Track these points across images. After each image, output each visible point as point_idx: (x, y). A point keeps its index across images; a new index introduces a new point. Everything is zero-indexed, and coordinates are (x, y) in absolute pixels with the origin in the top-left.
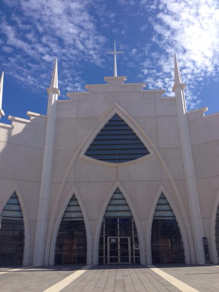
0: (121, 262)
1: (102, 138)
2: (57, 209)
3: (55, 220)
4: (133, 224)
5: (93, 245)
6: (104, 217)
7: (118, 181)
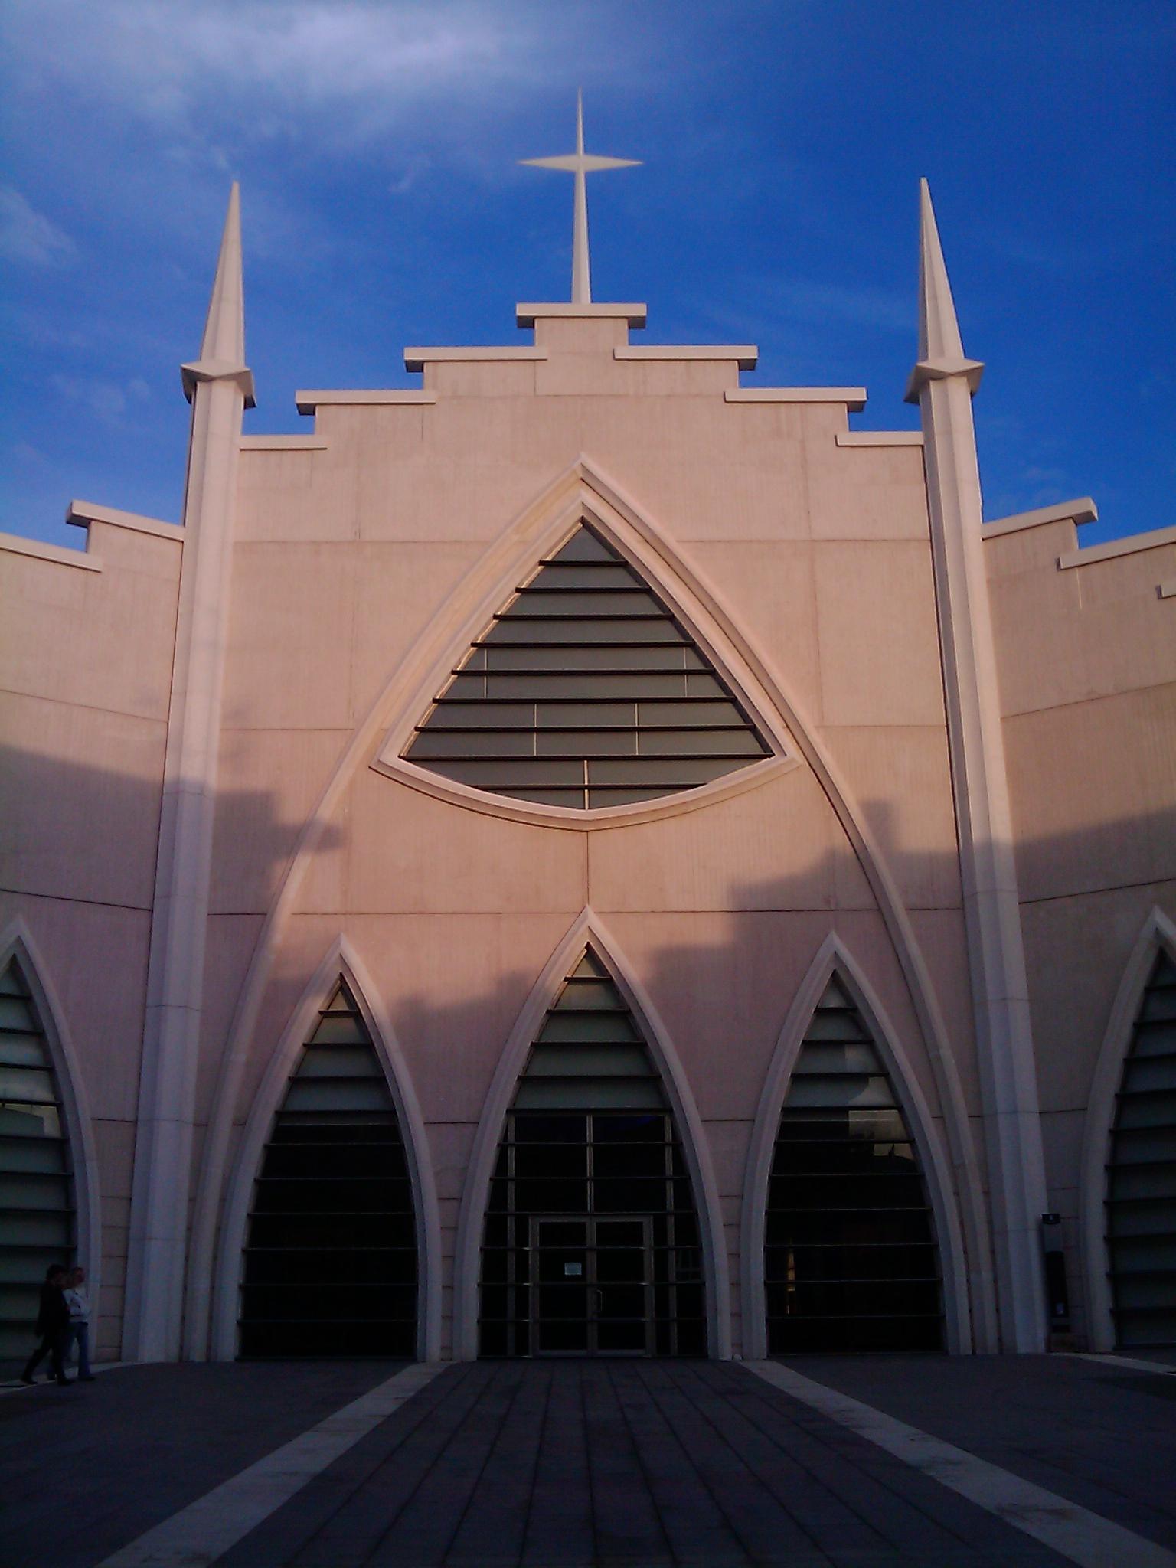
1: (483, 688)
3: (241, 1124)
4: (669, 1153)
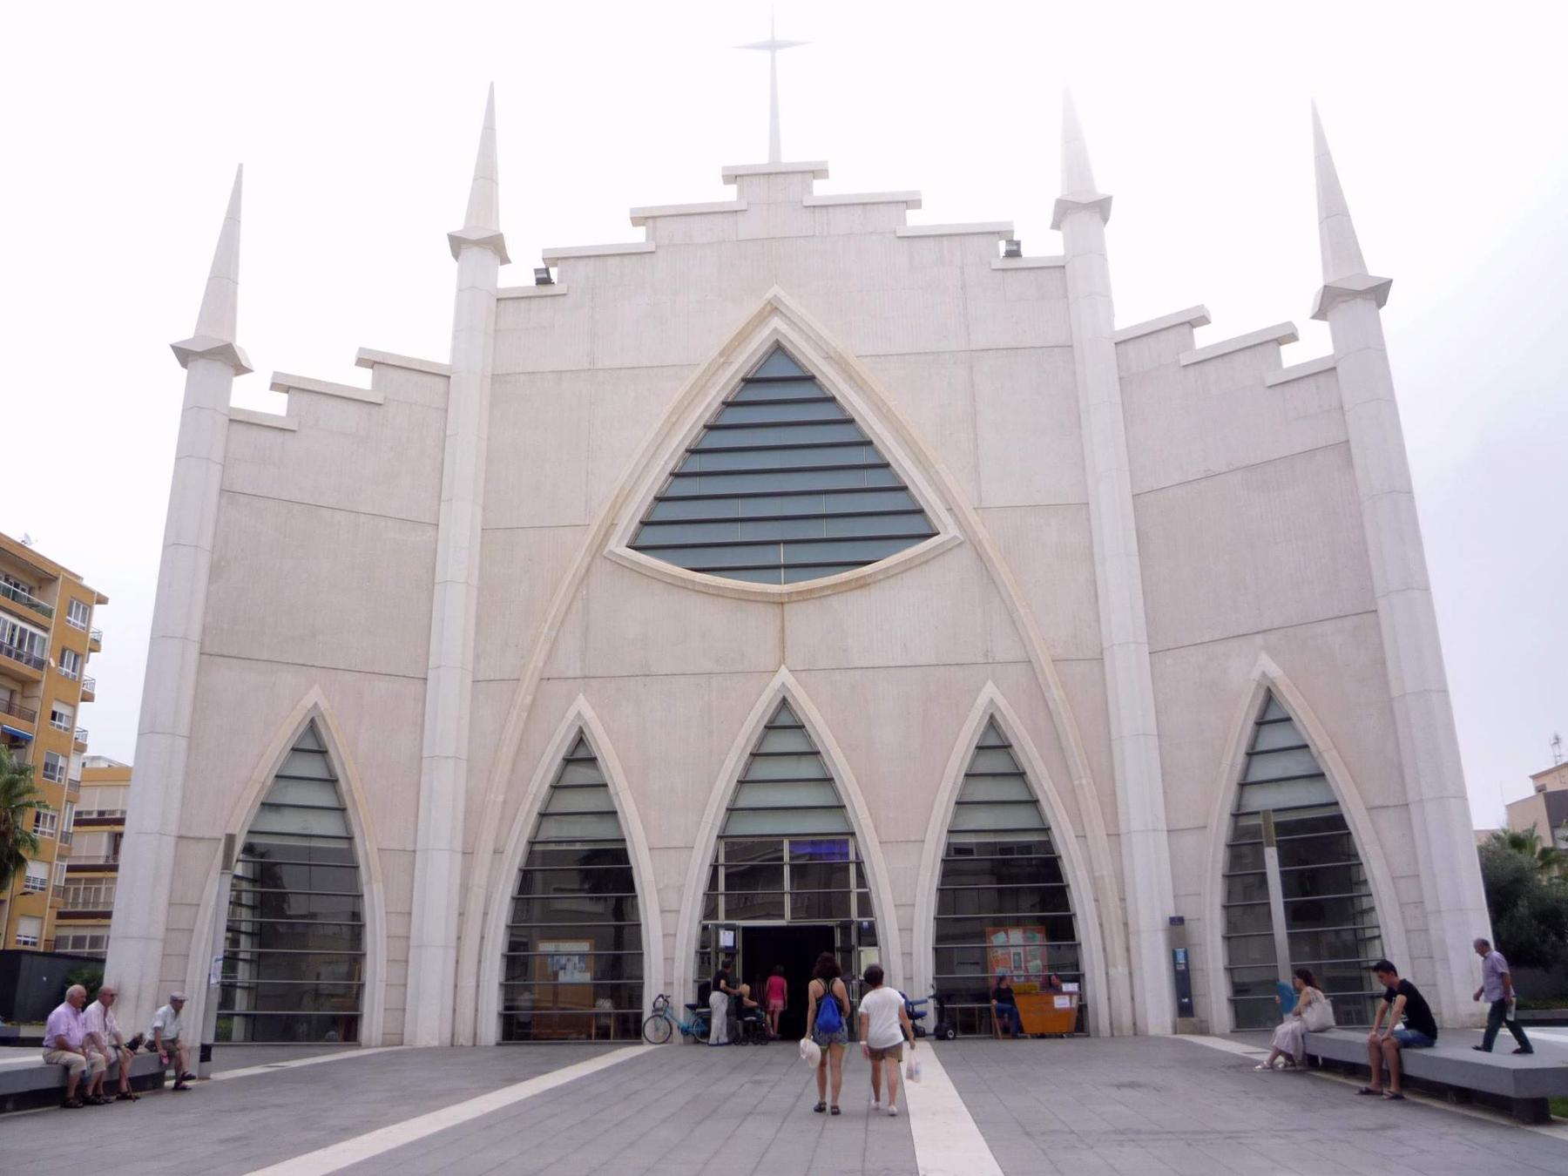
2: (505, 802)
3: (498, 852)
4: (853, 869)
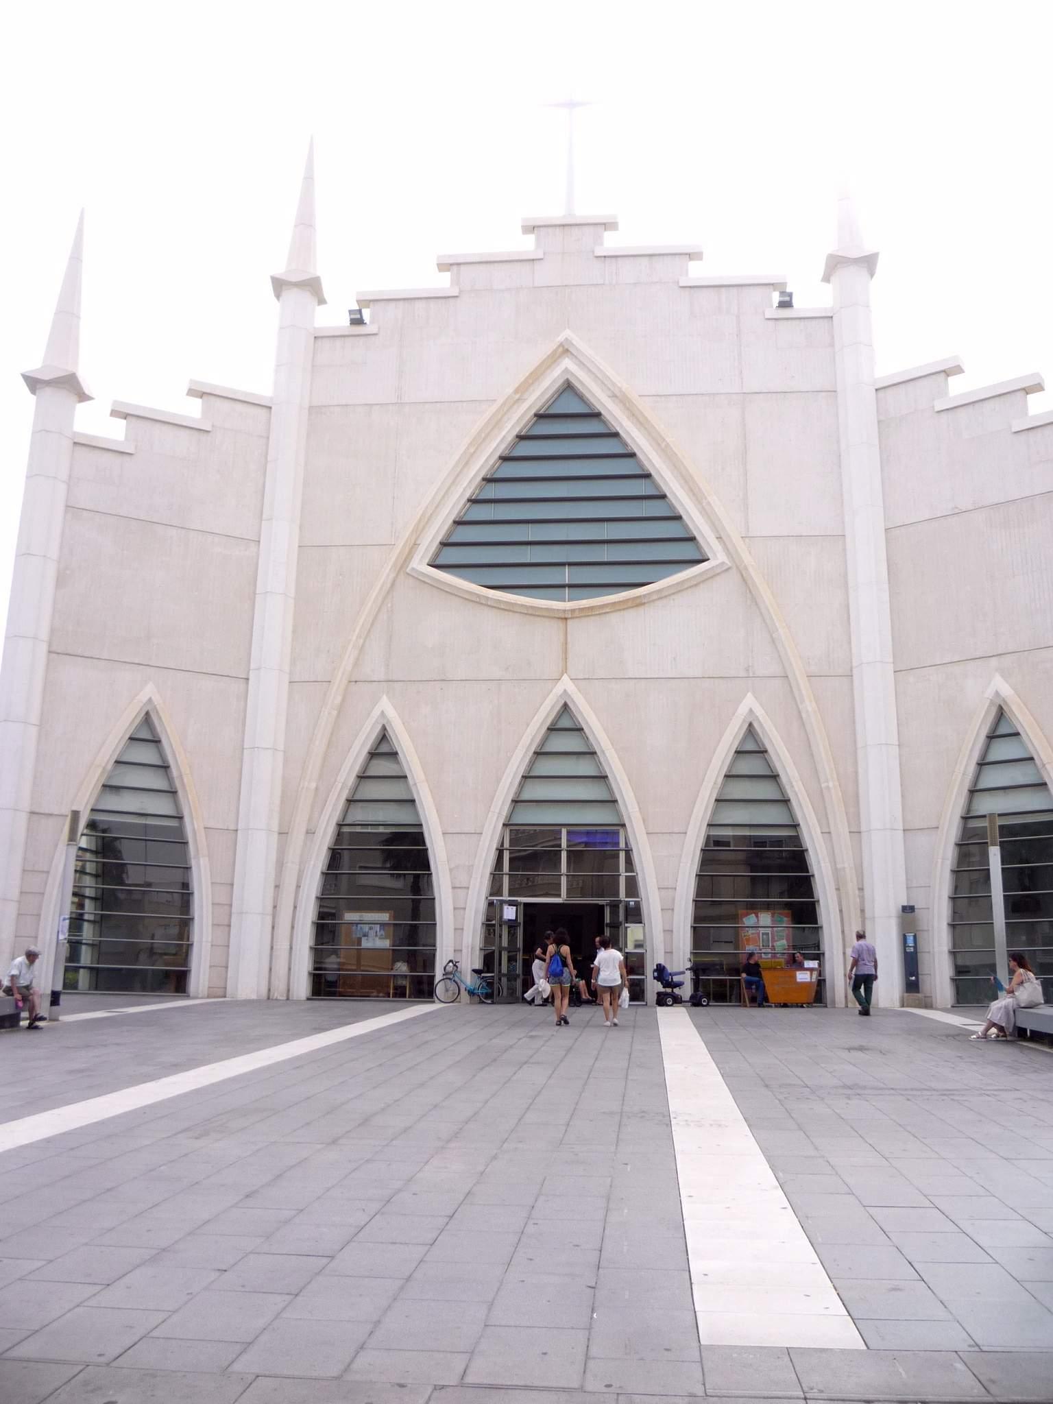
0: (566, 370)
2: (317, 789)
3: (310, 832)
4: (622, 855)
5: (459, 930)
6: (504, 825)
7: (565, 677)
